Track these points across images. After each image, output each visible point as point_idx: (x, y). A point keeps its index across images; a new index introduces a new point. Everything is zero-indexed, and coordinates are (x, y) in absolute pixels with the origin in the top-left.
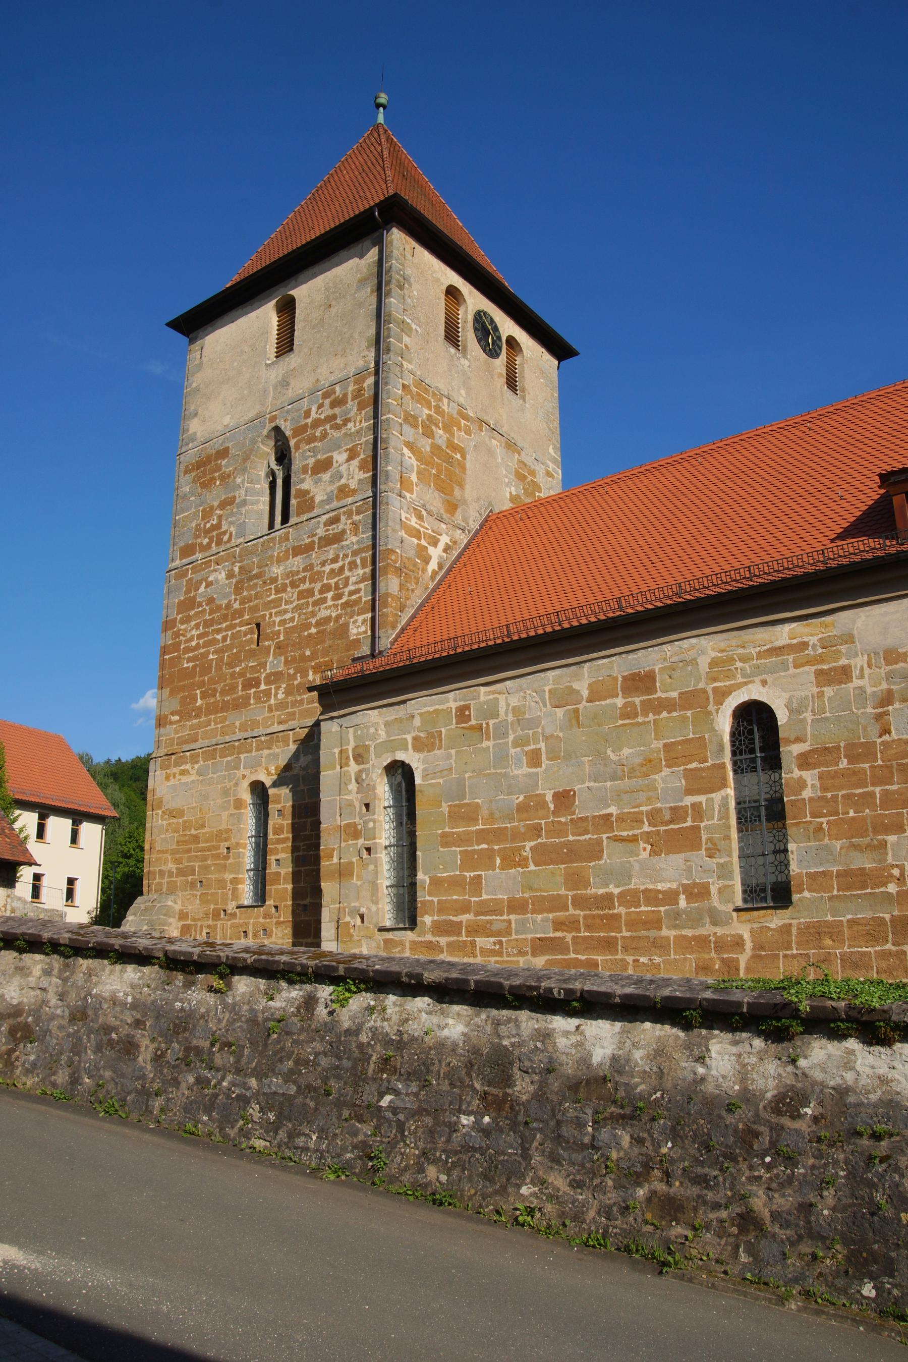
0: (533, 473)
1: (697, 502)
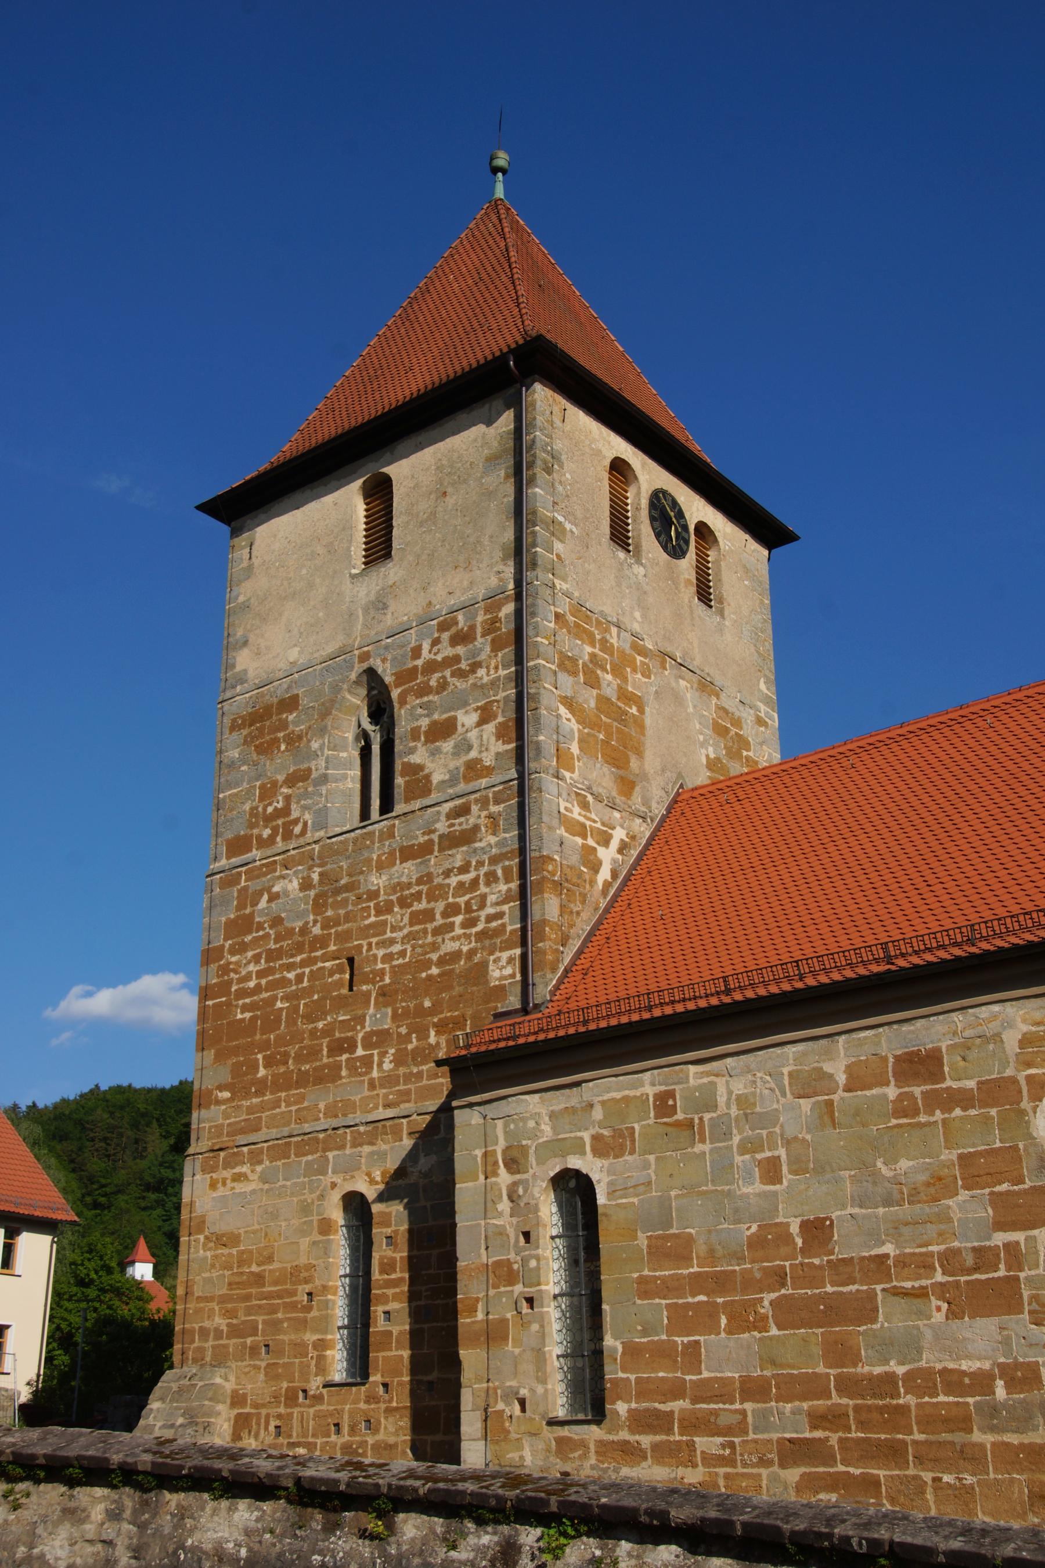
0: (737, 723)
1: (989, 789)
